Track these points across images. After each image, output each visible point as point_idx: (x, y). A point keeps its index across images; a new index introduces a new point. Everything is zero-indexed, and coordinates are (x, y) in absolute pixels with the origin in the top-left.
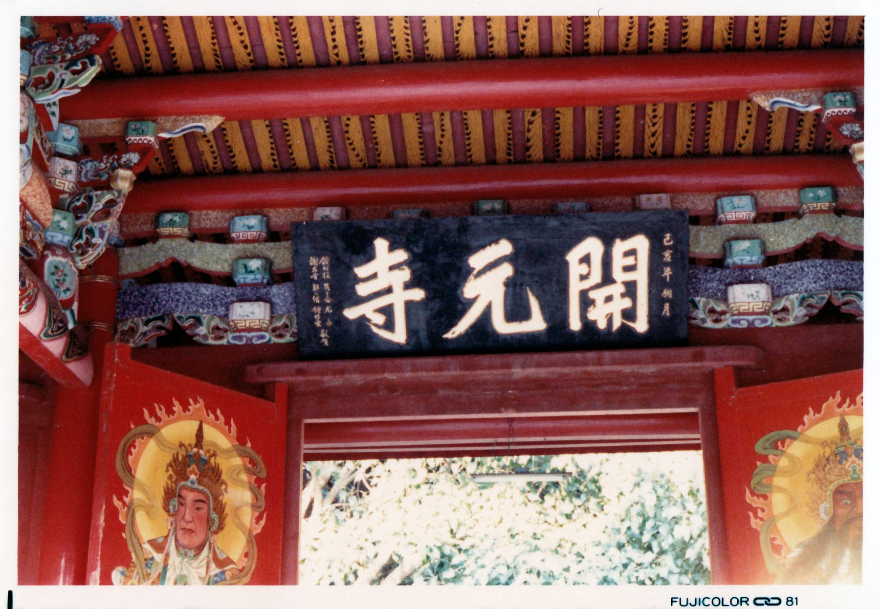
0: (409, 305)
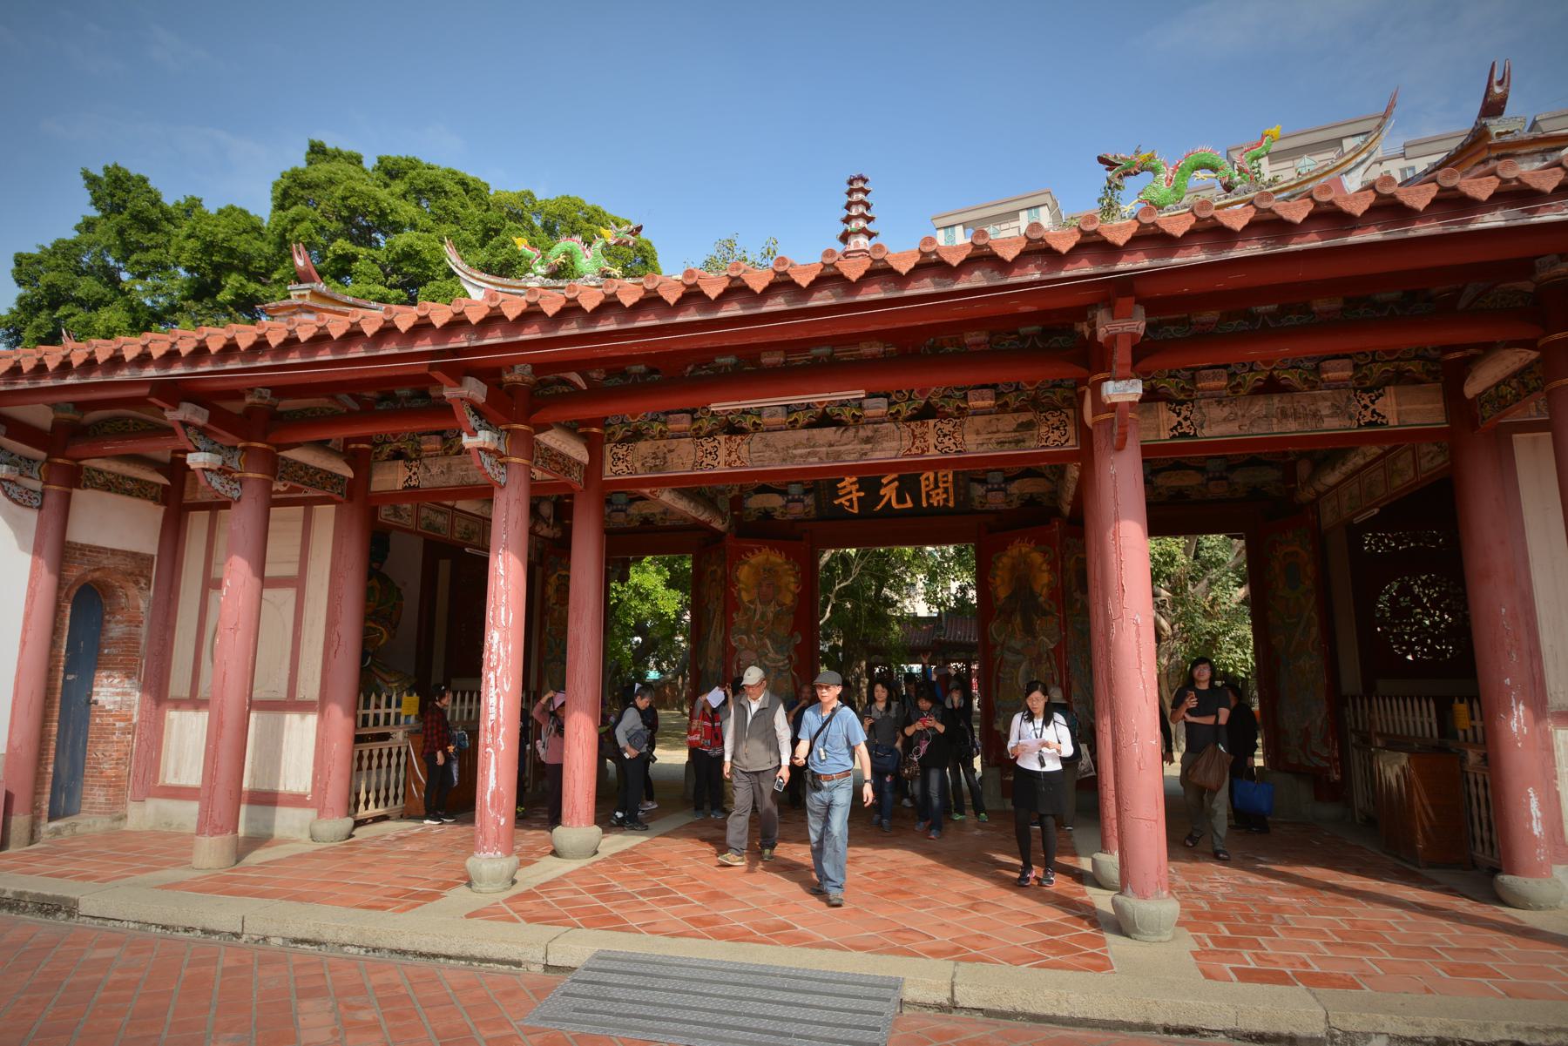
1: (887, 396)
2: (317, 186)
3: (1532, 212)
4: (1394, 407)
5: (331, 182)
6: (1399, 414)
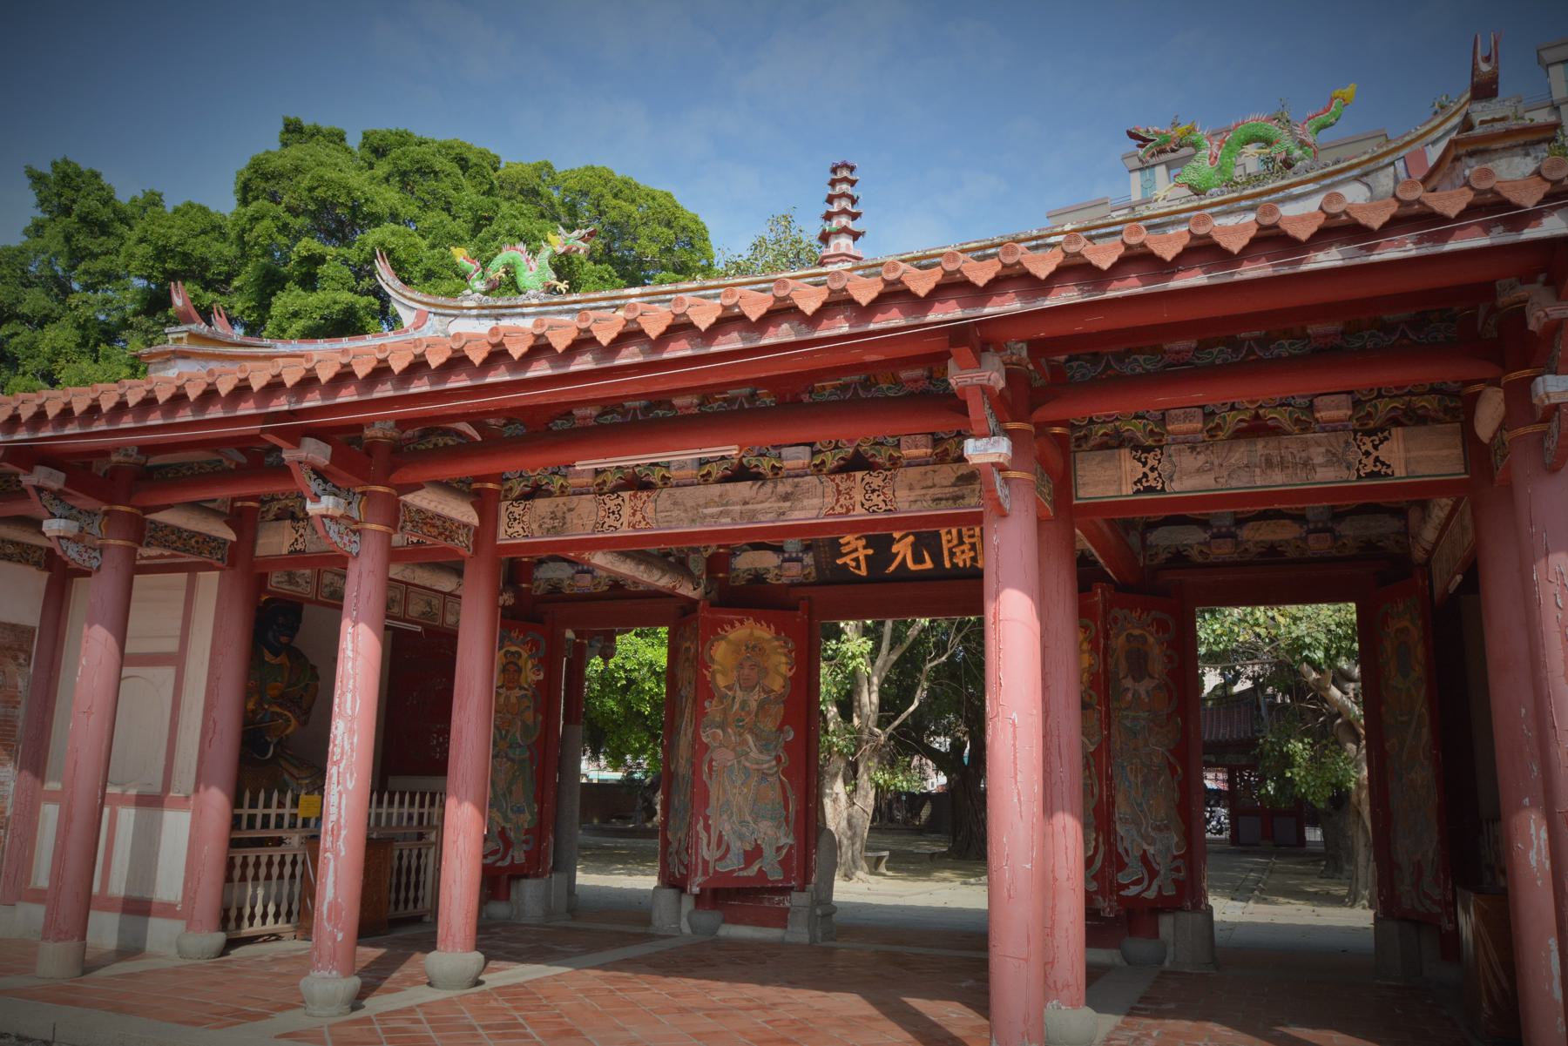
0: (867, 557)
1: (811, 445)
2: (281, 175)
4: (1402, 454)
6: (1407, 462)
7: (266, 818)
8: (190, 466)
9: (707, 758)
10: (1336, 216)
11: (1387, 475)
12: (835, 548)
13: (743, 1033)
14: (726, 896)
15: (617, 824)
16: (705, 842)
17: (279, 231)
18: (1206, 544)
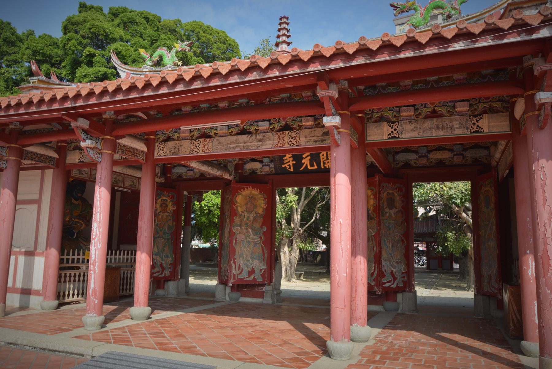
0: (293, 164)
1: (269, 120)
2: (79, 23)
3: (475, 42)
5: (84, 21)
6: (489, 127)
7: (73, 259)
8: (40, 130)
9: (234, 238)
10: (462, 29)
11: (481, 132)
12: (281, 160)
13: (243, 335)
14: (242, 287)
15: (208, 262)
16: (234, 268)
17: (78, 44)
18: (417, 159)
